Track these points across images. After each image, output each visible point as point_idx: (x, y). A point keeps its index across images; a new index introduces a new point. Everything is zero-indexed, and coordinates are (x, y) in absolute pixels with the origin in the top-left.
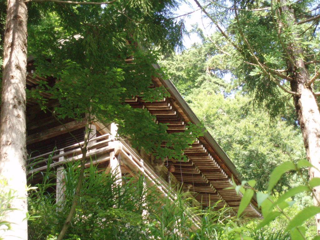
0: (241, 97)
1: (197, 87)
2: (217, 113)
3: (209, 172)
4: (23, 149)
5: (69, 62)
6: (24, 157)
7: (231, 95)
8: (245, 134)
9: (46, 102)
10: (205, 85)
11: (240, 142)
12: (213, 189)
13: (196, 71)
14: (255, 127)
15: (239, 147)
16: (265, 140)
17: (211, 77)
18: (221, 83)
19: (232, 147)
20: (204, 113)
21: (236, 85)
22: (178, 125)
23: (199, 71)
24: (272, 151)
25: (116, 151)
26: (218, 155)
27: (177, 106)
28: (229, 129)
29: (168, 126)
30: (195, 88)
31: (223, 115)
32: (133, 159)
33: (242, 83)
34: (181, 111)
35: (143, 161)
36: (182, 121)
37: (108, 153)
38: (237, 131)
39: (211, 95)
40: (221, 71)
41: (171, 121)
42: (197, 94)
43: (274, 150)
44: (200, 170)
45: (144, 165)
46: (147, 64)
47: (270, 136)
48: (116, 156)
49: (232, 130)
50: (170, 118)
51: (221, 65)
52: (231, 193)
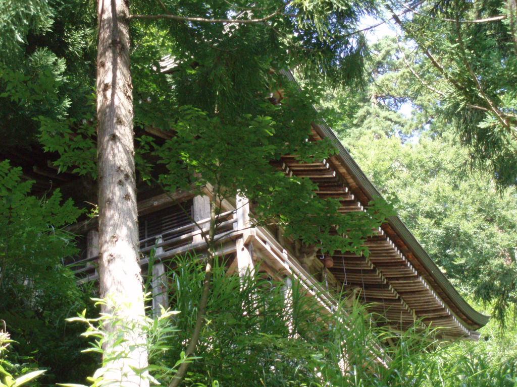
0: (428, 141)
1: (357, 126)
2: (390, 168)
3: (388, 266)
4: (136, 247)
5: (189, 109)
6: (137, 259)
7: (411, 138)
8: (438, 200)
9: (151, 170)
10: (369, 122)
11: (429, 215)
12: (393, 293)
13: (354, 100)
14: (453, 190)
15: (429, 223)
16: (471, 210)
17: (379, 110)
18: (395, 118)
19: (416, 223)
20: (369, 169)
21: (421, 122)
22: (339, 192)
23: (360, 100)
24: (482, 229)
25: (246, 237)
26: (401, 239)
27: (337, 163)
28: (411, 194)
29: (341, 202)
30: (353, 128)
31: (402, 170)
32: (272, 249)
33: (430, 119)
34: (343, 170)
35: (286, 252)
36: (345, 187)
37: (234, 240)
38: (425, 196)
39: (380, 140)
40: (395, 99)
41: (327, 186)
42: (358, 138)
43: (484, 226)
44: (374, 263)
45: (289, 258)
46: (304, 105)
47: (477, 203)
48: (247, 245)
49: (416, 194)
50: (325, 182)
51: (395, 90)
52: (422, 298)
